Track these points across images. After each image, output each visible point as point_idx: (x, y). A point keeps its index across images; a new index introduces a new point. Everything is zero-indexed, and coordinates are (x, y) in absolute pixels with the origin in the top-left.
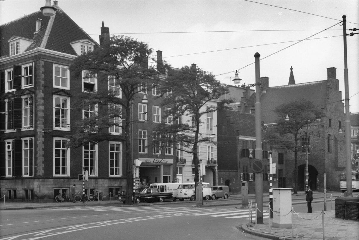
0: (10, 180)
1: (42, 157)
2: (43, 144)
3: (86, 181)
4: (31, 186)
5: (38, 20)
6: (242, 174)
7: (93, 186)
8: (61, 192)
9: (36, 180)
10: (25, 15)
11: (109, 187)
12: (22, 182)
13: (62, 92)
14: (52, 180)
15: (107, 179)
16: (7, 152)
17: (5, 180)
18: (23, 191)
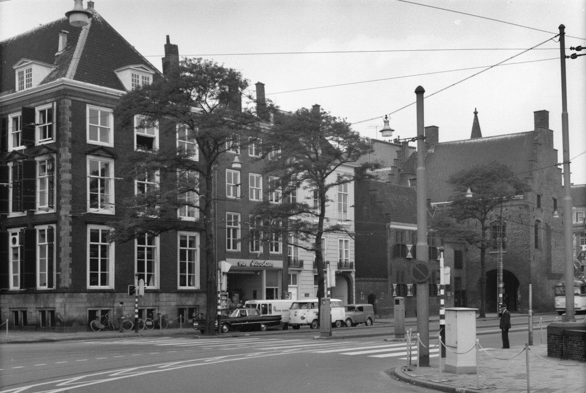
0: (16, 295)
1: (69, 258)
2: (70, 235)
3: (141, 296)
4: (51, 305)
5: (61, 32)
6: (395, 285)
7: (151, 304)
8: (99, 314)
9: (58, 295)
11: (178, 306)
12: (36, 298)
13: (100, 151)
14: (86, 294)
15: (175, 293)
16: (12, 249)
17: (8, 294)
18: (38, 312)
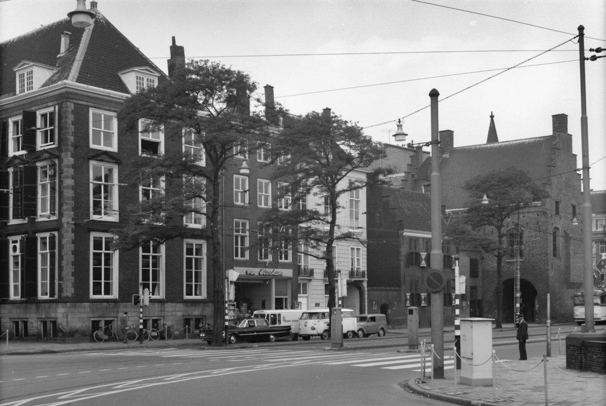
0: (17, 305)
1: (71, 266)
2: (73, 243)
3: (146, 306)
4: (53, 315)
5: (63, 33)
6: (408, 295)
7: (156, 314)
8: (102, 324)
9: (60, 305)
10: (42, 25)
11: (184, 316)
12: (38, 308)
13: (104, 156)
14: (89, 304)
15: (181, 302)
16: (12, 257)
17: (8, 304)
18: (39, 323)
